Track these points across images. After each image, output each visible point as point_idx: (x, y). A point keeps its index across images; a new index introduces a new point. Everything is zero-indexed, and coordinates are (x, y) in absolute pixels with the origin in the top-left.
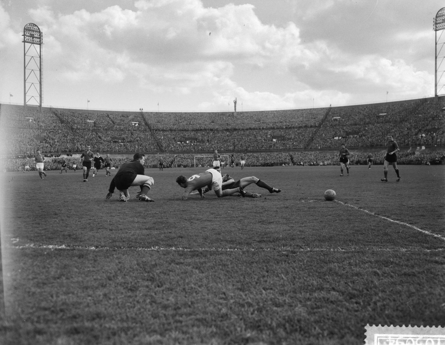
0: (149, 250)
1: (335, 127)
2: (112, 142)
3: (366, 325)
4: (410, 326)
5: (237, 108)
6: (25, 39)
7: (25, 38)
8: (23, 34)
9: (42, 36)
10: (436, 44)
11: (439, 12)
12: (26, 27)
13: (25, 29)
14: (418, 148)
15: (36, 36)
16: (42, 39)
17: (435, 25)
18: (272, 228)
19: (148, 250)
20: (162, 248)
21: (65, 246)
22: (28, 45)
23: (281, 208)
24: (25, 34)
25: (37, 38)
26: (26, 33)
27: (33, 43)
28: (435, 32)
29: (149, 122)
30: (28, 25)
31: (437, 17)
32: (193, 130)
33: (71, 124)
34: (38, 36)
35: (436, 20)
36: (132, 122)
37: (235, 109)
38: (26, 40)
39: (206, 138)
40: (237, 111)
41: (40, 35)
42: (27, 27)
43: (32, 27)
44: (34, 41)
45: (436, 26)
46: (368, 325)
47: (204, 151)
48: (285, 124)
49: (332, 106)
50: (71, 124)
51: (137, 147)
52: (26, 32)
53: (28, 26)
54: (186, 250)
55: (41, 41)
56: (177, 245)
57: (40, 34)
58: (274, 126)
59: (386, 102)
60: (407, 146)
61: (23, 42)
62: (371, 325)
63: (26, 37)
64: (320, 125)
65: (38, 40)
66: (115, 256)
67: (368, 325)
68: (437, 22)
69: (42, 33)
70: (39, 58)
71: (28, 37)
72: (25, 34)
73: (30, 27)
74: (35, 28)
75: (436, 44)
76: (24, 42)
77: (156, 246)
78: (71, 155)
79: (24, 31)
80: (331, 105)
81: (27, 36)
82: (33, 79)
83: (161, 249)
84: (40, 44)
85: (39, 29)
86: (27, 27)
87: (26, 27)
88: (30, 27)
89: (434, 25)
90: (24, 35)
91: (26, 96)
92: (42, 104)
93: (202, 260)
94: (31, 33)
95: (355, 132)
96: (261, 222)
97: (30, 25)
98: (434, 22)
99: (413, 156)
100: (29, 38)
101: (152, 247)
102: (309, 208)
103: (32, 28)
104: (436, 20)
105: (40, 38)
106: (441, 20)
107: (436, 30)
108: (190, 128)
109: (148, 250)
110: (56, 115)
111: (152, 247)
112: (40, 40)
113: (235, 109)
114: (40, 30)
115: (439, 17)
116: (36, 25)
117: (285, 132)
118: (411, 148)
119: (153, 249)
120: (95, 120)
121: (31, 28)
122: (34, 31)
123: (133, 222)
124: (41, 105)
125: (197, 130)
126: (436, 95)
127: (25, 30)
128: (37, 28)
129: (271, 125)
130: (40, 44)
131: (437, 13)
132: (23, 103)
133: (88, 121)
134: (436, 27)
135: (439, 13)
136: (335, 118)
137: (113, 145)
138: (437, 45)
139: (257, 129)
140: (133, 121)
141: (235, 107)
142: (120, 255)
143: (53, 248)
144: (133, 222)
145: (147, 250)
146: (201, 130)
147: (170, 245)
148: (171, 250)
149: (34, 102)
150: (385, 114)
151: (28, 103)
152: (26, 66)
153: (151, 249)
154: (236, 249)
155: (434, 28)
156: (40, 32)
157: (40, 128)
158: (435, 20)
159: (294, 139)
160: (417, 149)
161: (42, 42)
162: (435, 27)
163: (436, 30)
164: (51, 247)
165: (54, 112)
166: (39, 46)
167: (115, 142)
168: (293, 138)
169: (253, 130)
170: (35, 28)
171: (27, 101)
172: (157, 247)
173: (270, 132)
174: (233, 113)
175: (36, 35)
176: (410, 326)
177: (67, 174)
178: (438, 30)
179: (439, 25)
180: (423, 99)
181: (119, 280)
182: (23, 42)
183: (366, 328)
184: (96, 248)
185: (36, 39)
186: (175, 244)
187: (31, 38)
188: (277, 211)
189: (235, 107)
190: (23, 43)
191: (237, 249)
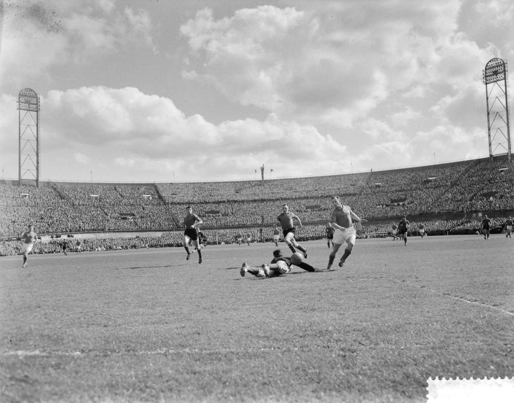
0: (154, 354)
1: (377, 194)
2: (120, 218)
5: (264, 175)
6: (20, 106)
7: (20, 105)
8: (18, 101)
9: (39, 102)
10: (487, 99)
11: (488, 63)
12: (21, 93)
14: (474, 215)
15: (33, 102)
16: (39, 105)
17: (485, 78)
18: (316, 317)
19: (153, 353)
20: (171, 350)
21: (40, 351)
22: (23, 112)
23: (326, 290)
24: (20, 101)
25: (34, 104)
26: (21, 100)
27: (29, 110)
28: (485, 85)
29: (163, 195)
30: (24, 90)
31: (486, 69)
32: (214, 203)
33: (73, 200)
34: (35, 102)
35: (485, 72)
36: (144, 196)
37: (263, 177)
38: (21, 107)
39: (230, 211)
40: (265, 179)
41: (37, 101)
42: (22, 93)
43: (28, 92)
44: (30, 108)
45: (486, 79)
47: (228, 225)
48: (320, 192)
49: (373, 171)
50: (73, 200)
51: (149, 223)
52: (21, 98)
53: (24, 92)
54: (204, 352)
55: (38, 108)
56: (193, 344)
57: (37, 100)
58: (308, 195)
59: (434, 164)
60: (462, 213)
61: (18, 109)
63: (21, 103)
65: (35, 106)
66: (106, 364)
68: (487, 74)
69: (39, 98)
70: (36, 127)
71: (23, 104)
72: (20, 101)
73: (26, 92)
74: (32, 93)
75: (487, 99)
76: (20, 109)
77: (164, 347)
78: (72, 236)
79: (19, 98)
80: (506, 63)
81: (22, 103)
83: (171, 351)
84: (37, 111)
85: (36, 94)
86: (22, 93)
87: (21, 93)
88: (26, 92)
89: (483, 78)
90: (19, 102)
91: (21, 170)
92: (40, 178)
93: (226, 367)
95: (401, 199)
96: (302, 309)
97: (26, 90)
98: (483, 74)
99: (469, 225)
100: (25, 104)
101: (158, 350)
102: (360, 289)
103: (28, 94)
104: (486, 73)
105: (37, 104)
106: (491, 72)
107: (486, 84)
108: (212, 199)
109: (153, 353)
110: (55, 189)
111: (158, 350)
112: (37, 107)
113: (263, 177)
114: (36, 96)
115: (489, 69)
116: (32, 90)
117: (321, 202)
118: (466, 215)
119: (159, 351)
120: (100, 194)
121: (27, 93)
122: (30, 97)
123: (137, 314)
124: (37, 180)
125: (219, 203)
126: (491, 156)
127: (20, 95)
128: (34, 93)
129: (305, 193)
130: (37, 111)
131: (487, 65)
133: (92, 195)
134: (486, 80)
135: (488, 65)
136: (377, 184)
137: (121, 223)
138: (489, 100)
140: (144, 194)
142: (112, 362)
143: (22, 355)
144: (137, 314)
145: (151, 354)
146: (224, 202)
147: (183, 346)
148: (184, 352)
149: (29, 175)
150: (434, 178)
151: (23, 178)
152: (21, 136)
153: (156, 352)
154: (272, 349)
155: (484, 81)
156: (37, 97)
157: (36, 205)
158: (484, 73)
159: (332, 209)
160: (473, 217)
161: (39, 109)
162: (485, 80)
163: (486, 84)
164: (20, 353)
165: (52, 186)
166: (36, 113)
167: (124, 218)
168: (330, 208)
169: (284, 200)
170: (32, 93)
171: (21, 175)
172: (164, 349)
173: (303, 202)
174: (260, 181)
175: (34, 101)
177: (67, 257)
178: (489, 83)
179: (489, 77)
180: (476, 160)
182: (18, 109)
184: (82, 353)
185: (33, 105)
186: (190, 344)
187: (27, 105)
188: (320, 294)
190: (18, 110)
191: (274, 348)
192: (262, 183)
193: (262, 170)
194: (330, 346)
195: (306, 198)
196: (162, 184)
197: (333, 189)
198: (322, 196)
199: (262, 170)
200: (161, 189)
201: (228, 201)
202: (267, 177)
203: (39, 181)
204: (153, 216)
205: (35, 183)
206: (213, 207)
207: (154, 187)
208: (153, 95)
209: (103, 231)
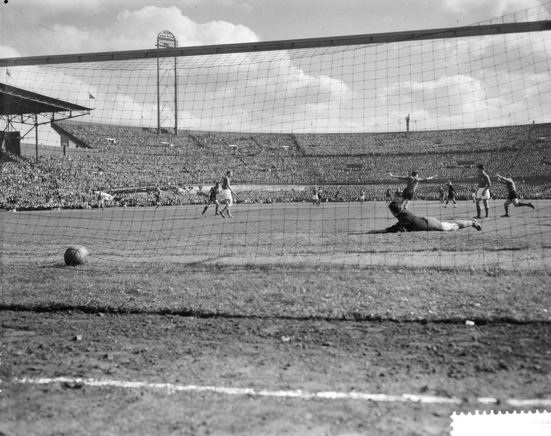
3: (452, 414)
4: (500, 412)
13: (158, 38)
37: (408, 129)
40: (410, 130)
46: (454, 413)
62: (458, 414)
64: (308, 156)
67: (454, 413)
82: (168, 95)
85: (174, 37)
92: (178, 126)
94: (165, 42)
108: (353, 152)
113: (408, 129)
116: (170, 33)
124: (176, 128)
125: (361, 156)
132: (157, 125)
139: (437, 153)
141: (408, 125)
156: (175, 41)
174: (405, 133)
176: (500, 412)
181: (51, 372)
183: (452, 417)
189: (408, 125)
192: (406, 135)
193: (408, 120)
194: (339, 280)
195: (458, 153)
196: (303, 136)
197: (485, 142)
198: (476, 151)
199: (408, 120)
200: (299, 140)
201: (371, 154)
202: (413, 127)
203: (178, 129)
204: (294, 169)
205: (174, 132)
206: (356, 161)
207: (292, 138)
208: (241, 26)
209: (244, 182)
